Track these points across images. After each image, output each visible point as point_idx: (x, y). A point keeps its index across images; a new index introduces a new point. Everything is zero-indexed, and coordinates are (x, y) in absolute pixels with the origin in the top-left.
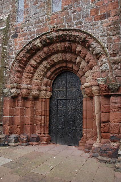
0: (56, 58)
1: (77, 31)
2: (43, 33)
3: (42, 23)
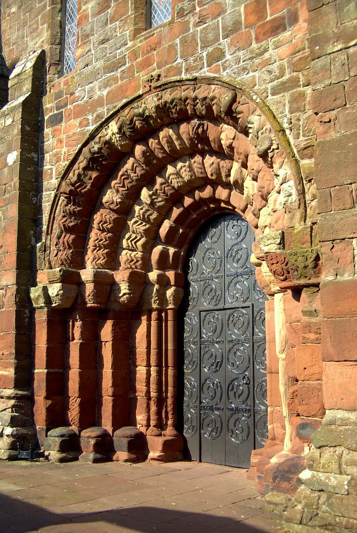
1: (210, 81)
2: (125, 101)
3: (120, 70)
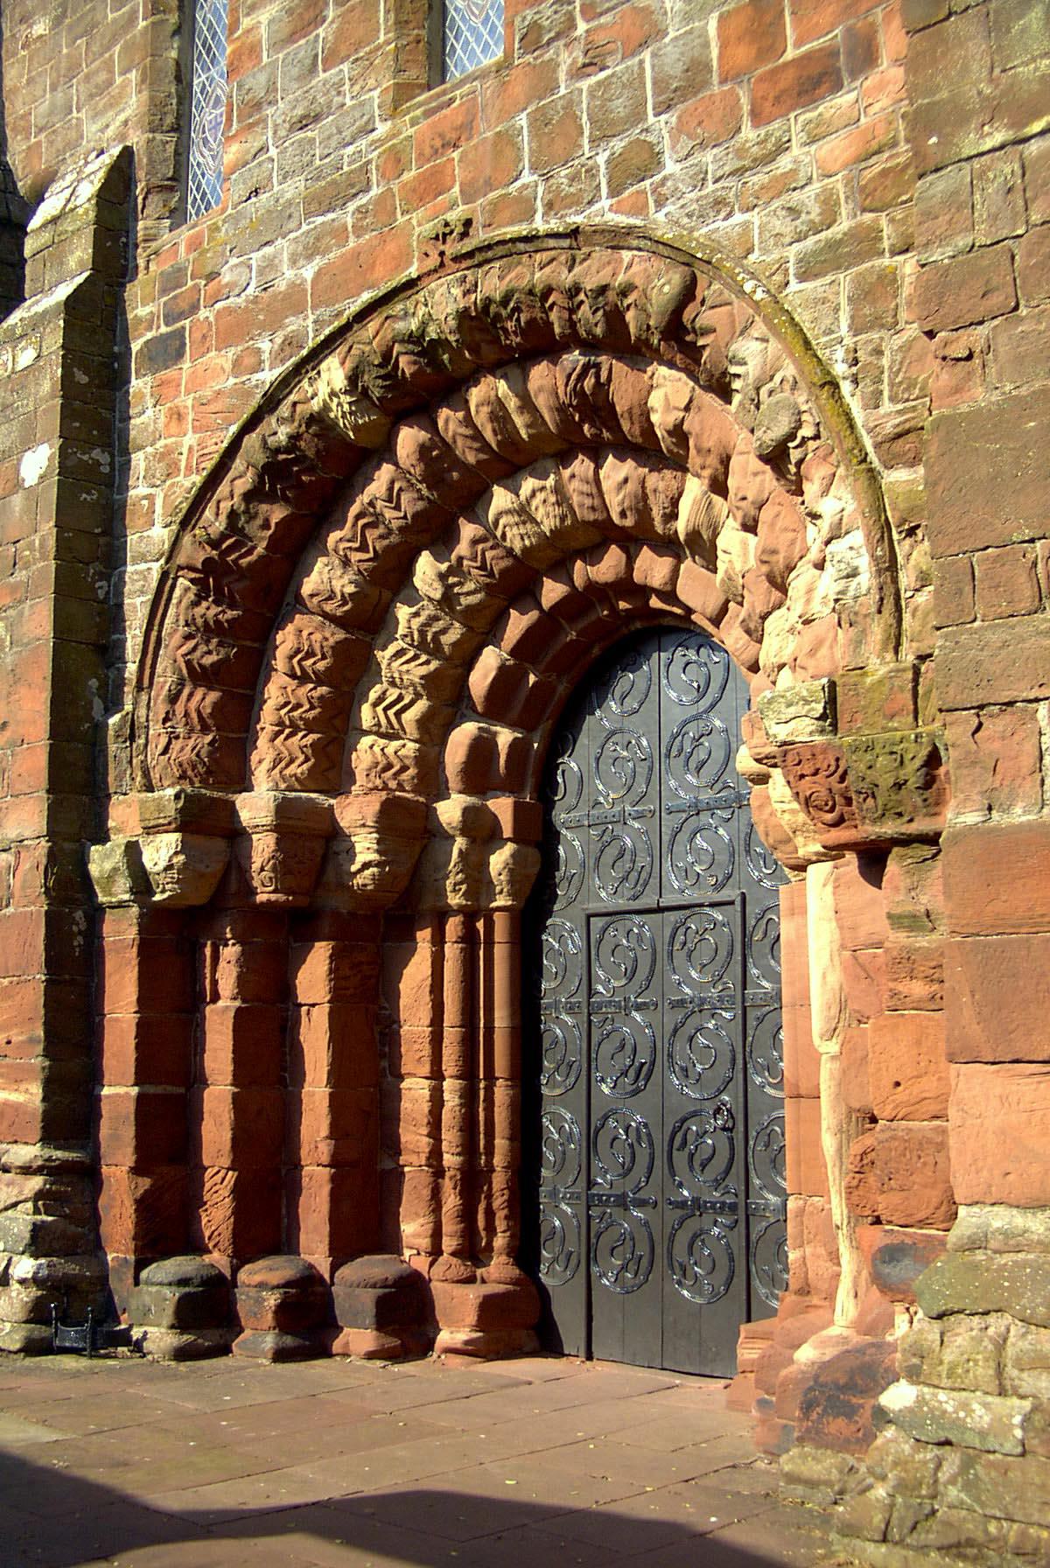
0: (522, 509)
1: (617, 239)
2: (366, 297)
3: (351, 206)
